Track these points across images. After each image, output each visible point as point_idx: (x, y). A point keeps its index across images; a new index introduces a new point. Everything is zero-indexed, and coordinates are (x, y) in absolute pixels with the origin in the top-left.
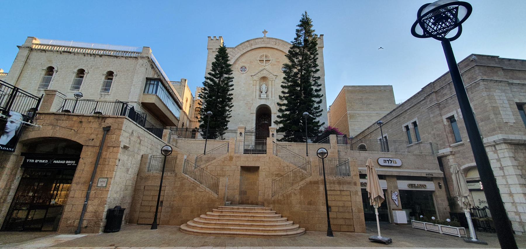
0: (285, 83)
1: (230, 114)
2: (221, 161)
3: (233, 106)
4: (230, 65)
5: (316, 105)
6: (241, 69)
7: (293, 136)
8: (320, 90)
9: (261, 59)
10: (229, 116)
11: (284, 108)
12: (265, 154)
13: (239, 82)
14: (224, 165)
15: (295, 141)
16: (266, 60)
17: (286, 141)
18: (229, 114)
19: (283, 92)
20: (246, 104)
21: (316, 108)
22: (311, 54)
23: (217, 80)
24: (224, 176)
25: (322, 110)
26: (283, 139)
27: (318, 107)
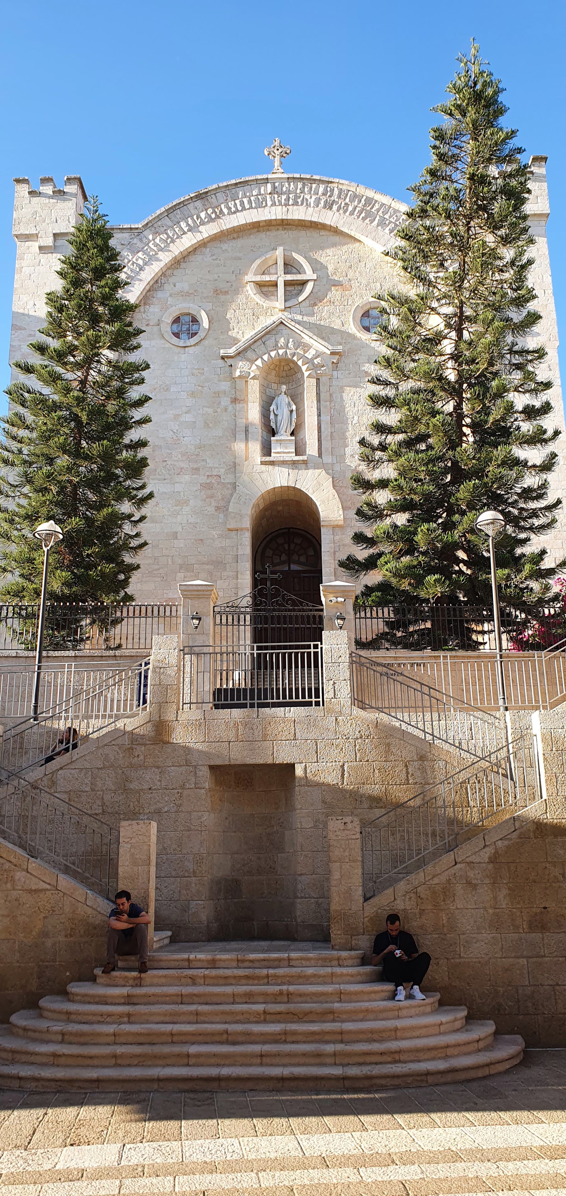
0: (386, 383)
1: (138, 535)
2: (120, 746)
3: (151, 496)
4: (132, 308)
5: (531, 481)
6: (175, 328)
7: (424, 620)
8: (546, 408)
9: (267, 278)
10: (134, 543)
11: (382, 497)
12: (317, 704)
13: (168, 390)
14: (131, 766)
15: (438, 645)
16: (287, 284)
17: (396, 643)
18: (132, 537)
19: (380, 428)
20: (207, 486)
21: (528, 494)
22: (506, 241)
23: (73, 376)
24: (133, 815)
25: (559, 502)
26: (383, 636)
27: (539, 488)
